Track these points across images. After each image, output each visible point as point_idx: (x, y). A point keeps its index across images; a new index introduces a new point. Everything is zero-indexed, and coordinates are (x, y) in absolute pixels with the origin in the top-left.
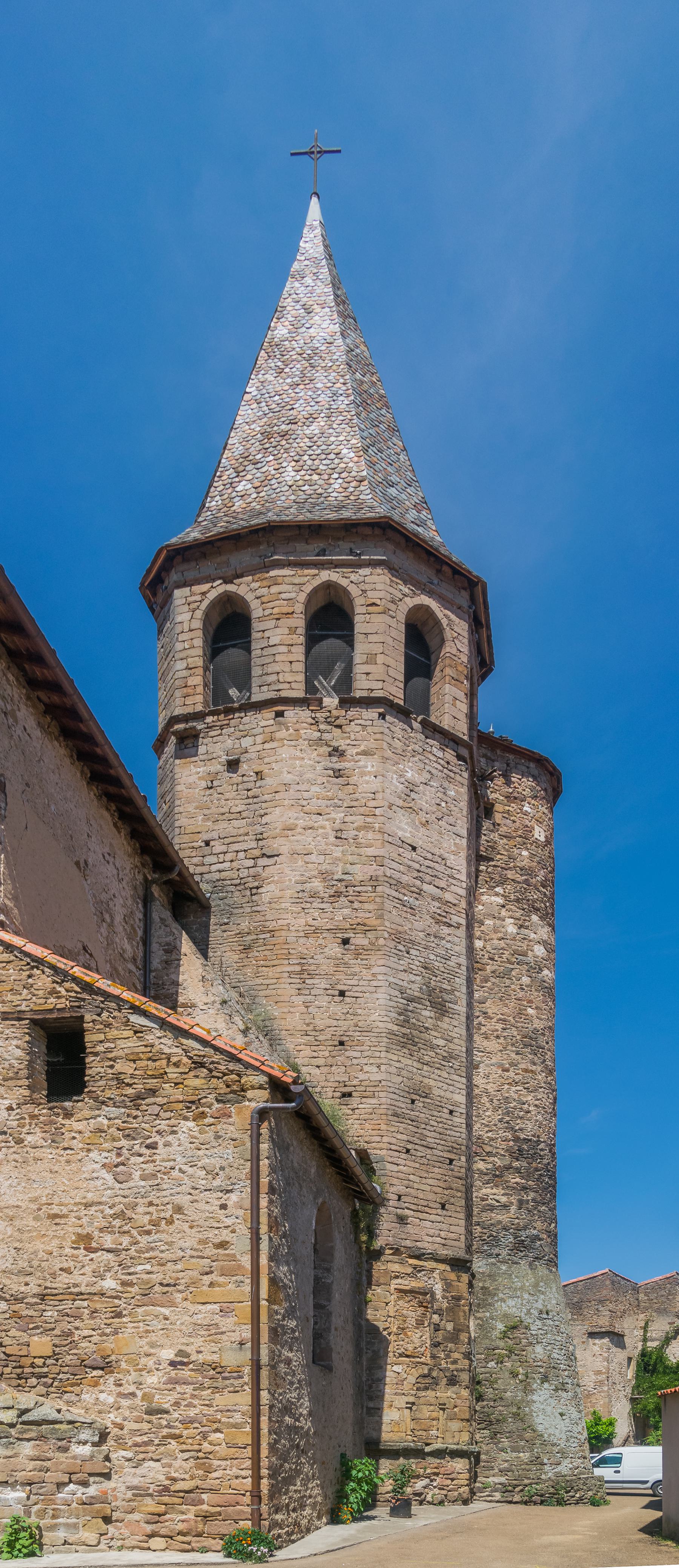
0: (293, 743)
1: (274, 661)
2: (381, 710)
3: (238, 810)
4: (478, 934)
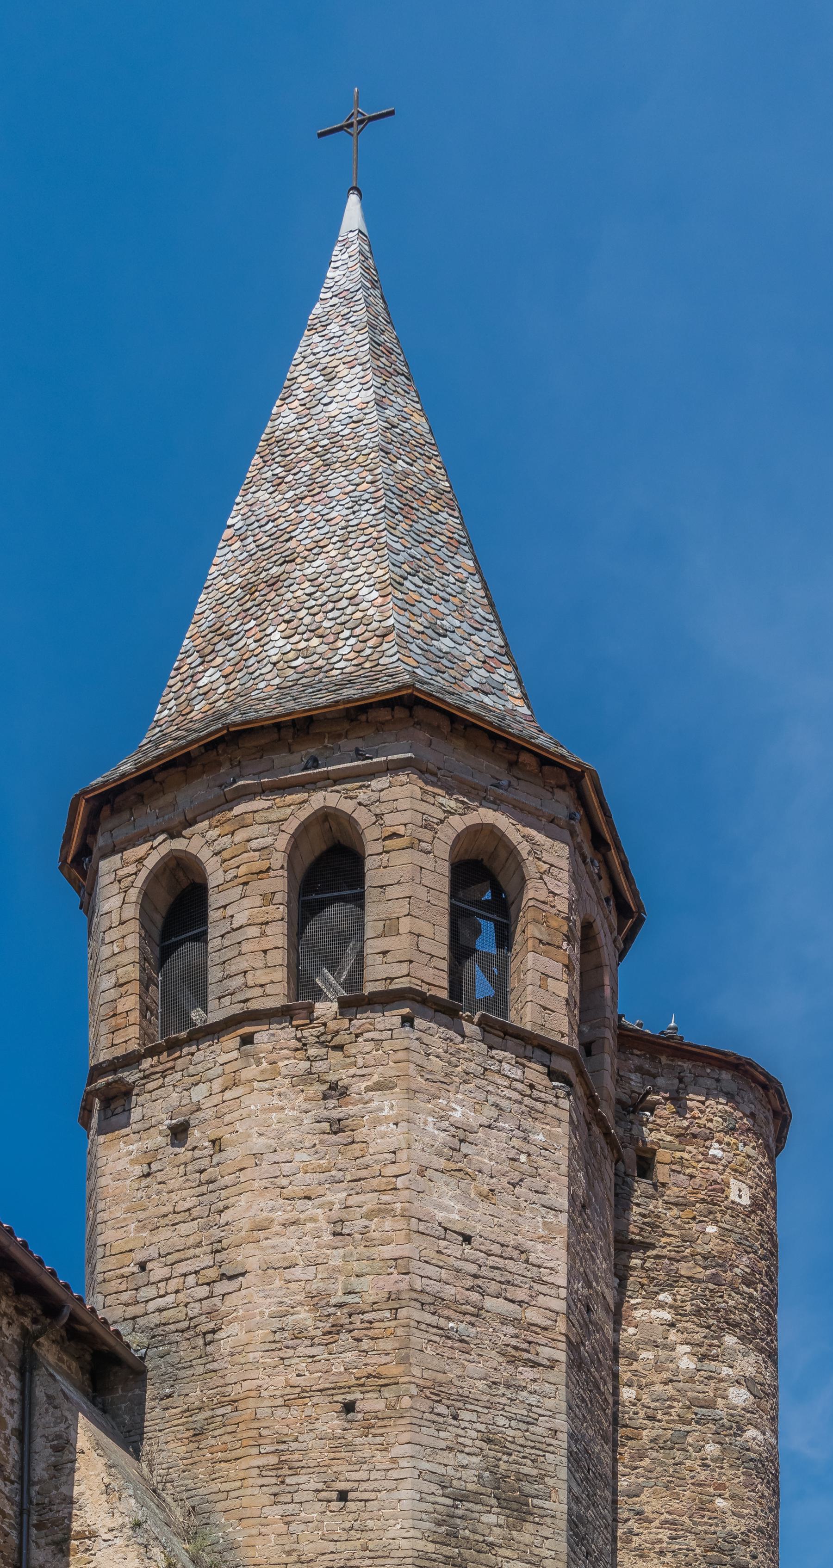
0: (266, 1085)
1: (240, 954)
2: (406, 1011)
3: (187, 1205)
4: (625, 1376)
